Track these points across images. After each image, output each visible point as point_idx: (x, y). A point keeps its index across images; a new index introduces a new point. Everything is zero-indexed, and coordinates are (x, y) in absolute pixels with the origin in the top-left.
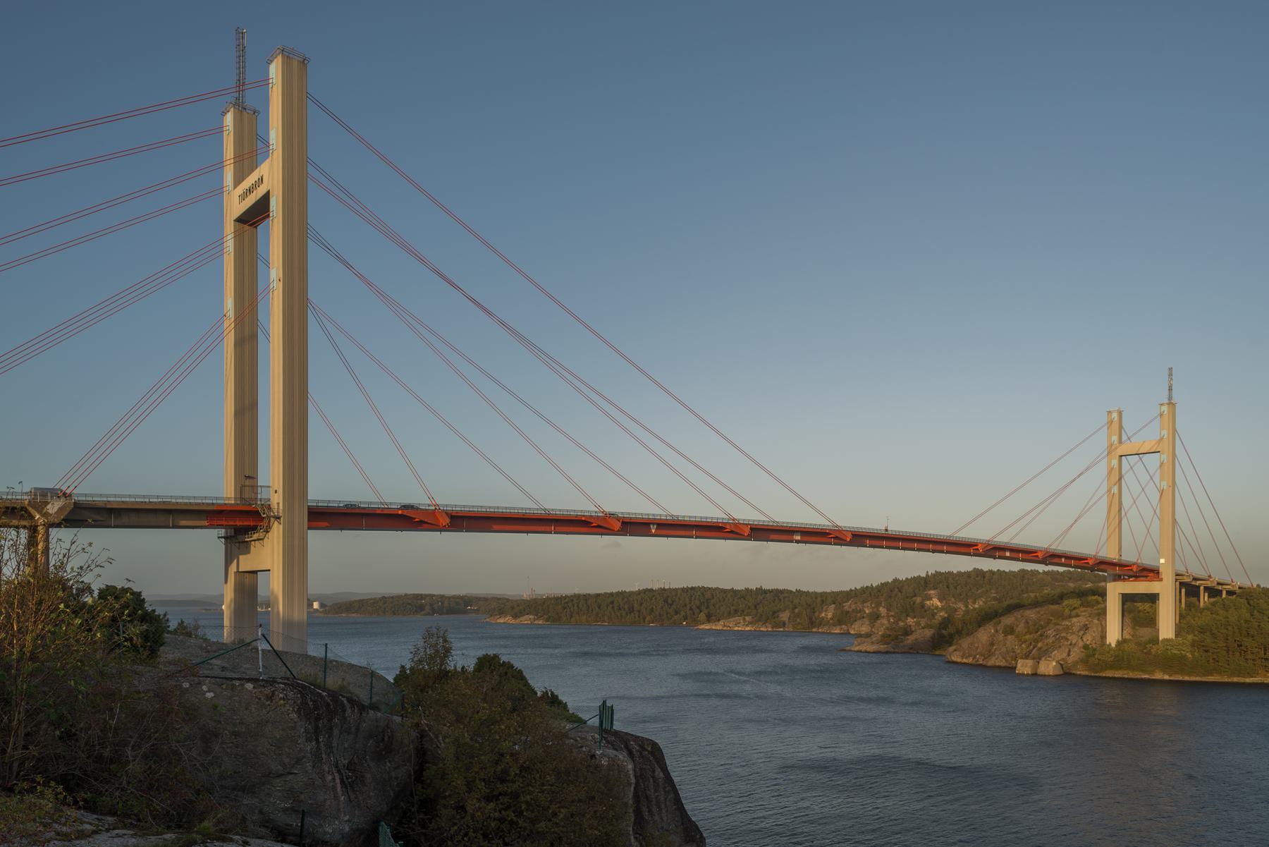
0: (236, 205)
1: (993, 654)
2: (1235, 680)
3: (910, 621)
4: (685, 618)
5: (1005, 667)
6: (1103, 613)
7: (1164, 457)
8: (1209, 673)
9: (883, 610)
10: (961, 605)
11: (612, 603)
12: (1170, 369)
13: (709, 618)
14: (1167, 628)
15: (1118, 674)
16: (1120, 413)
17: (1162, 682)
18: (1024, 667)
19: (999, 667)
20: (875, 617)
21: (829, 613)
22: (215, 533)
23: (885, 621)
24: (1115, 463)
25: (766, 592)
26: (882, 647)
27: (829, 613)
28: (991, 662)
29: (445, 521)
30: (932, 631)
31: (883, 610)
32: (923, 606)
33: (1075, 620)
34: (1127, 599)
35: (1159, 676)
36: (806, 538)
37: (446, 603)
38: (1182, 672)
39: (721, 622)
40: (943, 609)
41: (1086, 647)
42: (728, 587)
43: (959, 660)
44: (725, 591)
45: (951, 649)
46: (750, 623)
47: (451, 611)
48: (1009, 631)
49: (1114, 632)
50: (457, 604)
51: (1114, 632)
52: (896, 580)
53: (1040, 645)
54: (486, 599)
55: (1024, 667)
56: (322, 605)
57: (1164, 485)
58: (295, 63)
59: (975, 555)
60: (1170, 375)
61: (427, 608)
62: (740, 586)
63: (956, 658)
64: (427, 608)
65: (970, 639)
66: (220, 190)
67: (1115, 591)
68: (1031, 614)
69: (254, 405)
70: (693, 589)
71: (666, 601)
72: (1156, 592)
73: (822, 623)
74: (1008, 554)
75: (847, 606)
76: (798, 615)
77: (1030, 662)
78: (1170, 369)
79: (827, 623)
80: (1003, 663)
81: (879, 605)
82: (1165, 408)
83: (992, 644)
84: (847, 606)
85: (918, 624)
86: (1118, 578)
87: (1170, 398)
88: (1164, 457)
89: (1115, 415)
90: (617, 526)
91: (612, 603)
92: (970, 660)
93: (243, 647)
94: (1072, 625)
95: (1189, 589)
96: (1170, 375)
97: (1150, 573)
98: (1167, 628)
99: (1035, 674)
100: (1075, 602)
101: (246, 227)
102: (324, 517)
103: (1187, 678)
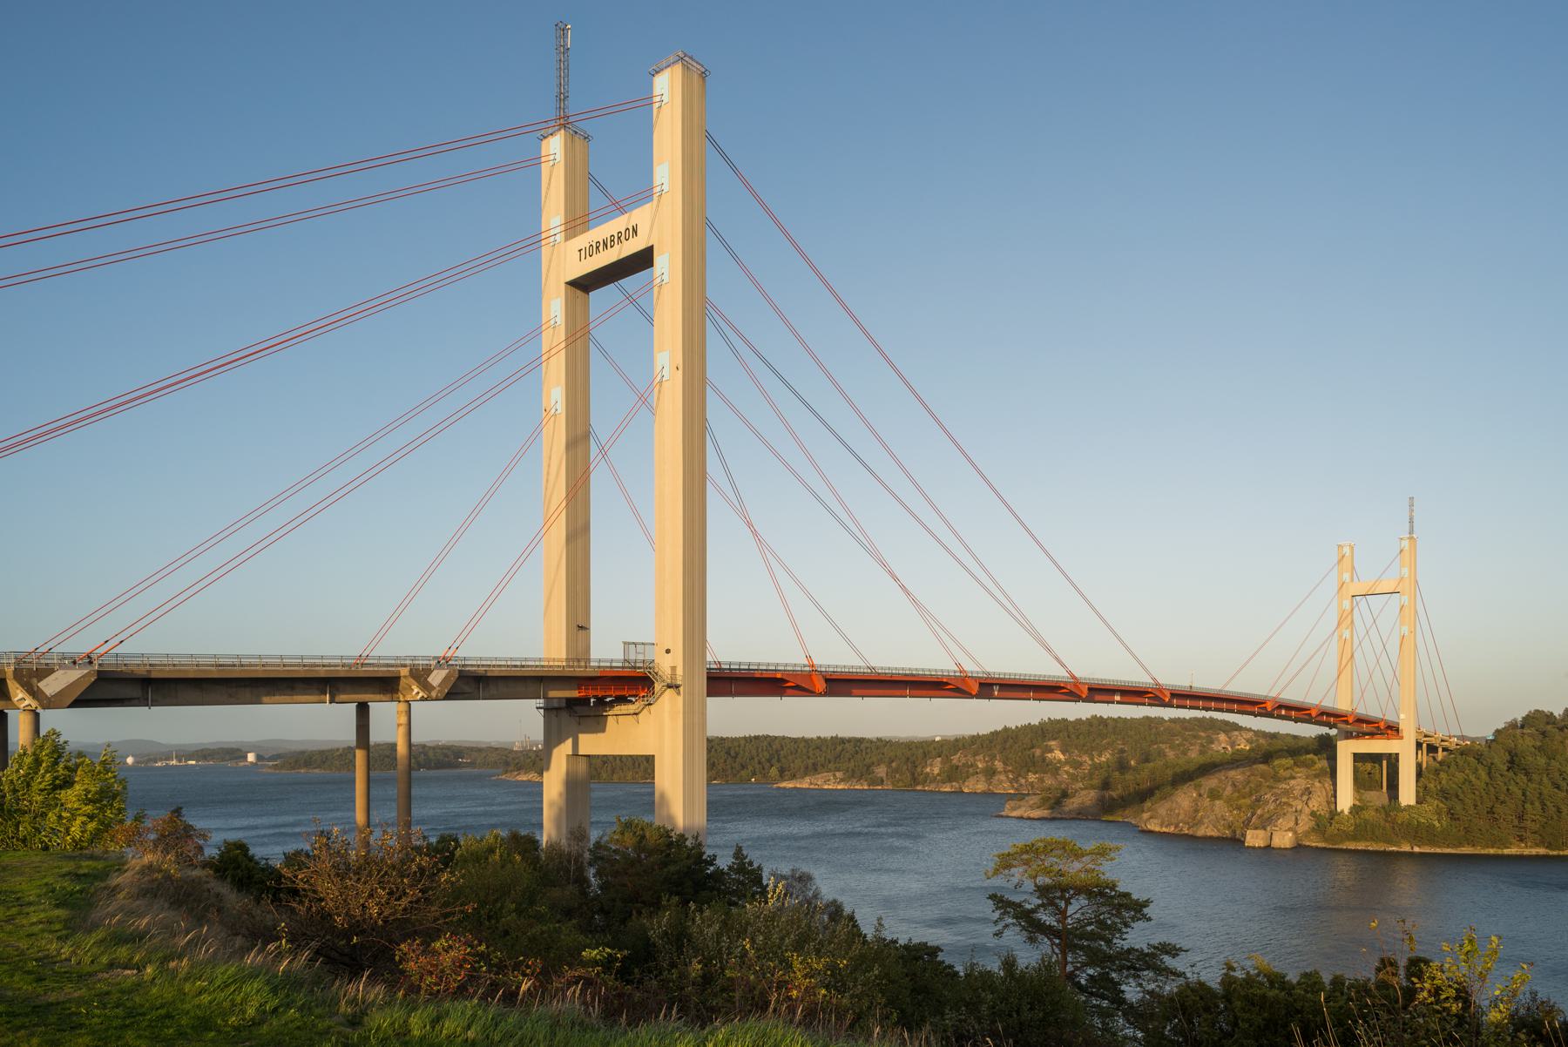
0: (568, 258)
1: (1201, 822)
2: (1492, 851)
3: (1032, 777)
4: (754, 774)
5: (1218, 838)
7: (1405, 599)
8: (1460, 845)
9: (999, 765)
10: (1086, 758)
12: (1411, 499)
13: (782, 774)
14: (1407, 794)
15: (1361, 846)
16: (1352, 548)
17: (1411, 854)
18: (1254, 838)
19: (1211, 838)
20: (990, 773)
21: (935, 767)
22: (534, 703)
23: (1003, 777)
24: (1347, 604)
25: (843, 741)
26: (1045, 813)
27: (935, 767)
28: (1201, 832)
29: (821, 685)
30: (1093, 794)
31: (999, 765)
32: (1044, 760)
33: (1293, 782)
34: (1358, 758)
35: (1406, 848)
36: (1126, 699)
37: (431, 754)
38: (1432, 843)
39: (807, 779)
40: (1067, 762)
41: (1313, 814)
42: (814, 736)
43: (1157, 829)
44: (795, 740)
45: (1146, 816)
46: (842, 780)
47: (440, 765)
48: (1214, 795)
49: (1346, 799)
50: (446, 756)
51: (1346, 799)
52: (1006, 729)
53: (1259, 812)
54: (480, 750)
55: (1254, 838)
56: (259, 757)
57: (1405, 630)
58: (696, 77)
60: (1412, 505)
62: (811, 734)
63: (1154, 826)
65: (1167, 805)
66: (533, 241)
67: (1346, 750)
68: (1237, 775)
69: (586, 528)
70: (756, 738)
71: (728, 753)
73: (927, 779)
74: (1117, 698)
76: (896, 770)
77: (1261, 833)
78: (1411, 499)
79: (934, 780)
80: (1215, 833)
81: (993, 758)
82: (1406, 544)
83: (1197, 811)
84: (957, 759)
85: (1041, 780)
86: (1348, 736)
87: (1411, 532)
88: (1405, 599)
89: (1347, 550)
90: (975, 689)
92: (1172, 829)
94: (1292, 789)
95: (1427, 746)
96: (1412, 505)
97: (1392, 730)
98: (1407, 794)
99: (1269, 846)
100: (1289, 761)
101: (579, 293)
102: (725, 682)
103: (1438, 850)
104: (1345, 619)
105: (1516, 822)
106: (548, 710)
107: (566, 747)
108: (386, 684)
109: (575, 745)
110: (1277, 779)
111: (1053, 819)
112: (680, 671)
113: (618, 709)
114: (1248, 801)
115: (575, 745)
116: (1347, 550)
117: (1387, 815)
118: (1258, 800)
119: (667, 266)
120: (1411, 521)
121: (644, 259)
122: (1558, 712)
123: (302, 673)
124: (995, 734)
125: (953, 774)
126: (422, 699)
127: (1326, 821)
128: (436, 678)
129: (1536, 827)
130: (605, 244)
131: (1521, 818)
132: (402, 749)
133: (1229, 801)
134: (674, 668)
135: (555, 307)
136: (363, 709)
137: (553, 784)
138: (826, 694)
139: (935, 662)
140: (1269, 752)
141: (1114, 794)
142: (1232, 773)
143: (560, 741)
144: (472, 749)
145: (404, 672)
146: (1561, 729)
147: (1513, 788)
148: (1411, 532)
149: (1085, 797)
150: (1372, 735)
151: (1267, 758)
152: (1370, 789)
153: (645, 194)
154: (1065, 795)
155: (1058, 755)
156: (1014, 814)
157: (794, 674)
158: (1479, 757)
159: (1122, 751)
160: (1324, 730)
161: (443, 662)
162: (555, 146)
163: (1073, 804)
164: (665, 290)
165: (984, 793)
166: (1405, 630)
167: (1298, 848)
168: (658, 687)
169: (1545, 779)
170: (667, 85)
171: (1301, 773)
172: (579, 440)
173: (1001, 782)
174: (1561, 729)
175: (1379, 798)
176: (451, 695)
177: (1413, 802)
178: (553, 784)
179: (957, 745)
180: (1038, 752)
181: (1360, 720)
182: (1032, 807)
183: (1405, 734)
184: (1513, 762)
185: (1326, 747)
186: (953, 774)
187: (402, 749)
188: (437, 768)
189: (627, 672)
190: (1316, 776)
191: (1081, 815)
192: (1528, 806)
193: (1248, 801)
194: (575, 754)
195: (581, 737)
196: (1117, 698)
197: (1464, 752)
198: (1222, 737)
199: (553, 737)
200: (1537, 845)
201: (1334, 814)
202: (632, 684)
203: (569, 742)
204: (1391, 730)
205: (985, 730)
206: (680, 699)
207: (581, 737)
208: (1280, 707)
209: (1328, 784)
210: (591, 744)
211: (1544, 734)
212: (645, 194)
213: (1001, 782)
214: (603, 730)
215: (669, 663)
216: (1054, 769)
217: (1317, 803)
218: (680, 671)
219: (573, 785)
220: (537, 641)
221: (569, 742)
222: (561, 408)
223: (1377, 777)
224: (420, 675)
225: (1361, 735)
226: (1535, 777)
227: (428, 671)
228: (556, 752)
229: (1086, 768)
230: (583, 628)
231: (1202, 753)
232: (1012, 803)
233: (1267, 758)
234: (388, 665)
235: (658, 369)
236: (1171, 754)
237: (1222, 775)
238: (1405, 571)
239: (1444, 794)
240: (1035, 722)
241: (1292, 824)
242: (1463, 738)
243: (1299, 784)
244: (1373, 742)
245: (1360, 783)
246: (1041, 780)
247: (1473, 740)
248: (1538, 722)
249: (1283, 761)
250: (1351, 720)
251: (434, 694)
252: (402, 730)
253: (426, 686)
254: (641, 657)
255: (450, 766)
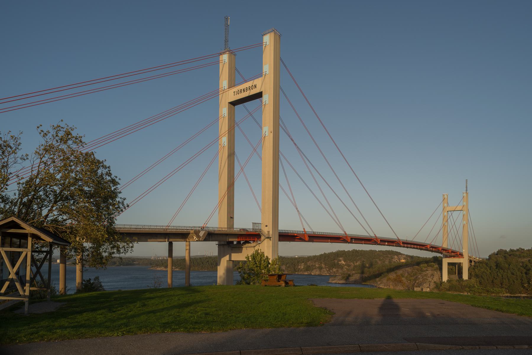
3: (334, 270)
6: (441, 269)
7: (465, 212)
9: (323, 265)
10: (352, 263)
11: (208, 261)
12: (467, 180)
14: (465, 276)
16: (447, 196)
21: (302, 266)
23: (325, 270)
24: (446, 214)
27: (302, 266)
29: (307, 238)
30: (359, 275)
31: (323, 265)
33: (427, 272)
34: (449, 264)
37: (124, 260)
40: (346, 265)
41: (435, 282)
47: (127, 264)
49: (445, 278)
51: (445, 278)
52: (325, 254)
54: (141, 259)
57: (465, 222)
59: (425, 250)
60: (467, 182)
61: (118, 263)
64: (118, 263)
67: (446, 262)
68: (409, 269)
72: (461, 262)
73: (299, 270)
74: (386, 244)
75: (308, 264)
78: (467, 180)
79: (302, 270)
81: (321, 263)
82: (465, 194)
84: (309, 263)
85: (337, 271)
86: (446, 257)
87: (467, 191)
88: (465, 212)
89: (446, 196)
91: (208, 261)
93: (65, 294)
94: (427, 274)
96: (467, 182)
98: (465, 276)
100: (426, 265)
104: (446, 220)
105: (500, 285)
106: (219, 245)
107: (227, 258)
108: (183, 235)
109: (230, 257)
110: (422, 271)
111: (347, 284)
112: (271, 233)
113: (247, 245)
114: (413, 278)
115: (230, 257)
116: (446, 196)
117: (459, 283)
118: (416, 278)
119: (267, 98)
120: (467, 187)
121: (259, 95)
122: (530, 248)
123: (174, 231)
124: (321, 255)
125: (308, 268)
126: (197, 241)
127: (439, 285)
128: (201, 234)
129: (506, 287)
130: (244, 90)
131: (502, 284)
132: (187, 258)
133: (406, 278)
134: (269, 232)
135: (224, 111)
136: (171, 244)
137: (221, 270)
138: (309, 241)
139: (336, 230)
140: (417, 262)
141: (366, 275)
142: (407, 269)
143: (224, 256)
144: (138, 259)
145: (192, 232)
146: (510, 255)
147: (499, 274)
148: (467, 191)
149: (356, 277)
150: (454, 257)
151: (418, 264)
152: (452, 274)
153: (260, 74)
154: (349, 275)
155: (343, 262)
156: (333, 282)
157: (300, 234)
158: (487, 264)
159: (364, 261)
160: (438, 255)
161: (203, 228)
162: (225, 58)
163: (352, 279)
164: (266, 106)
165: (318, 275)
166: (465, 222)
167: (431, 292)
168: (263, 238)
169: (509, 272)
170: (268, 39)
171: (429, 269)
172: (231, 155)
173: (324, 271)
174: (510, 255)
175: (455, 277)
176: (205, 240)
177: (467, 279)
178: (221, 270)
179: (309, 259)
180: (336, 261)
181: (453, 252)
182: (339, 280)
183: (465, 256)
184: (497, 265)
185: (438, 262)
186: (308, 268)
187: (187, 258)
188: (127, 265)
189: (254, 233)
190: (435, 270)
191: (355, 282)
192: (504, 280)
193: (413, 278)
194: (230, 260)
195: (232, 254)
196: (386, 244)
197: (480, 262)
198: (396, 257)
199: (221, 254)
200: (507, 293)
201: (442, 283)
202: (254, 236)
203: (228, 256)
204: (461, 255)
205: (318, 254)
206: (271, 242)
207: (232, 254)
208: (432, 247)
209: (439, 273)
210: (236, 257)
211: (505, 257)
212: (260, 74)
213: (324, 271)
214: (241, 252)
215: (267, 229)
216: (341, 267)
217: (436, 279)
218: (271, 233)
219: (228, 271)
220: (217, 223)
221: (228, 256)
222: (226, 144)
223: (454, 270)
224: (197, 233)
225: (450, 257)
226: (506, 271)
227: (199, 231)
228: (222, 260)
229: (352, 267)
230: (232, 218)
231: (390, 262)
232: (332, 278)
233: (418, 264)
234: (140, 229)
235: (264, 133)
236: (380, 262)
237: (404, 269)
238: (465, 203)
239: (477, 276)
240: (346, 250)
241: (428, 286)
242: (480, 258)
243: (429, 272)
244: (454, 259)
245: (450, 272)
246: (337, 271)
247: (483, 259)
248: (501, 252)
249: (424, 265)
250: (450, 251)
251: (201, 239)
252: (187, 251)
253: (198, 236)
254: (257, 228)
255: (131, 264)
